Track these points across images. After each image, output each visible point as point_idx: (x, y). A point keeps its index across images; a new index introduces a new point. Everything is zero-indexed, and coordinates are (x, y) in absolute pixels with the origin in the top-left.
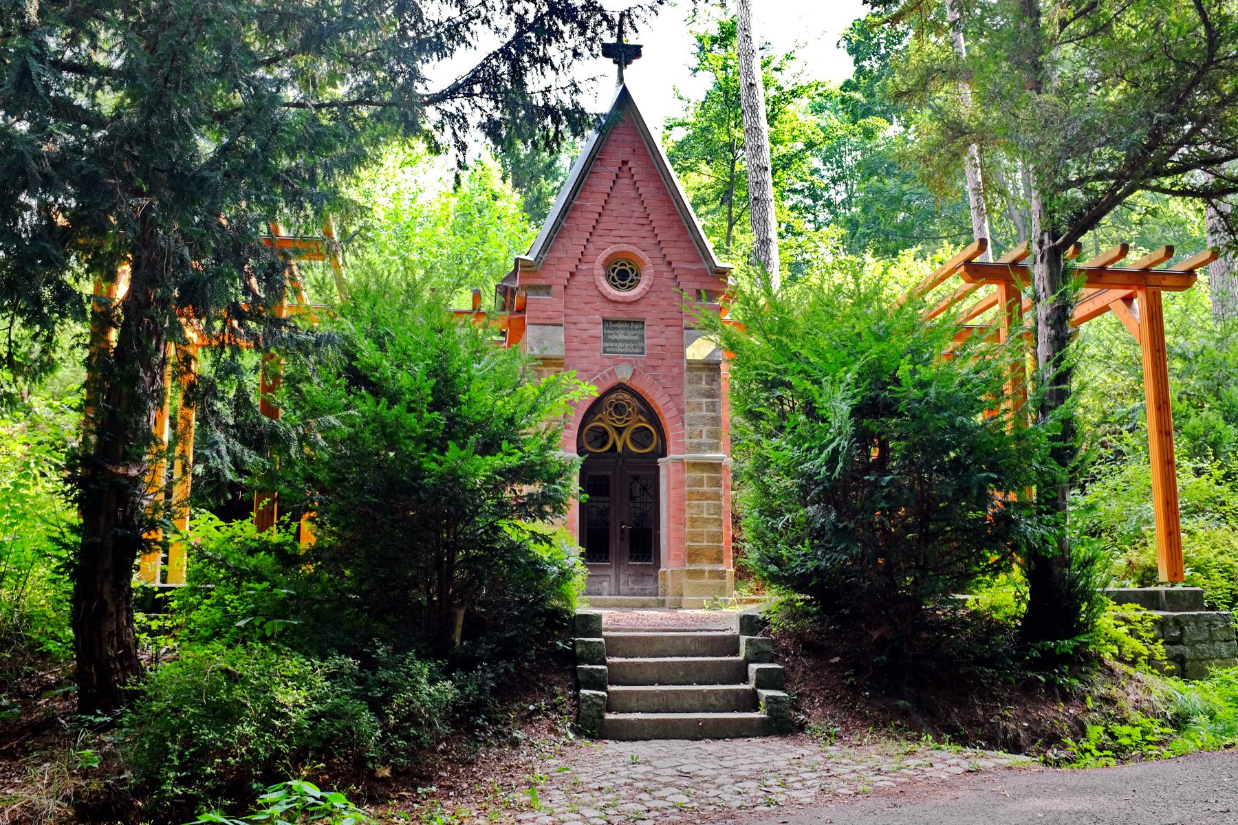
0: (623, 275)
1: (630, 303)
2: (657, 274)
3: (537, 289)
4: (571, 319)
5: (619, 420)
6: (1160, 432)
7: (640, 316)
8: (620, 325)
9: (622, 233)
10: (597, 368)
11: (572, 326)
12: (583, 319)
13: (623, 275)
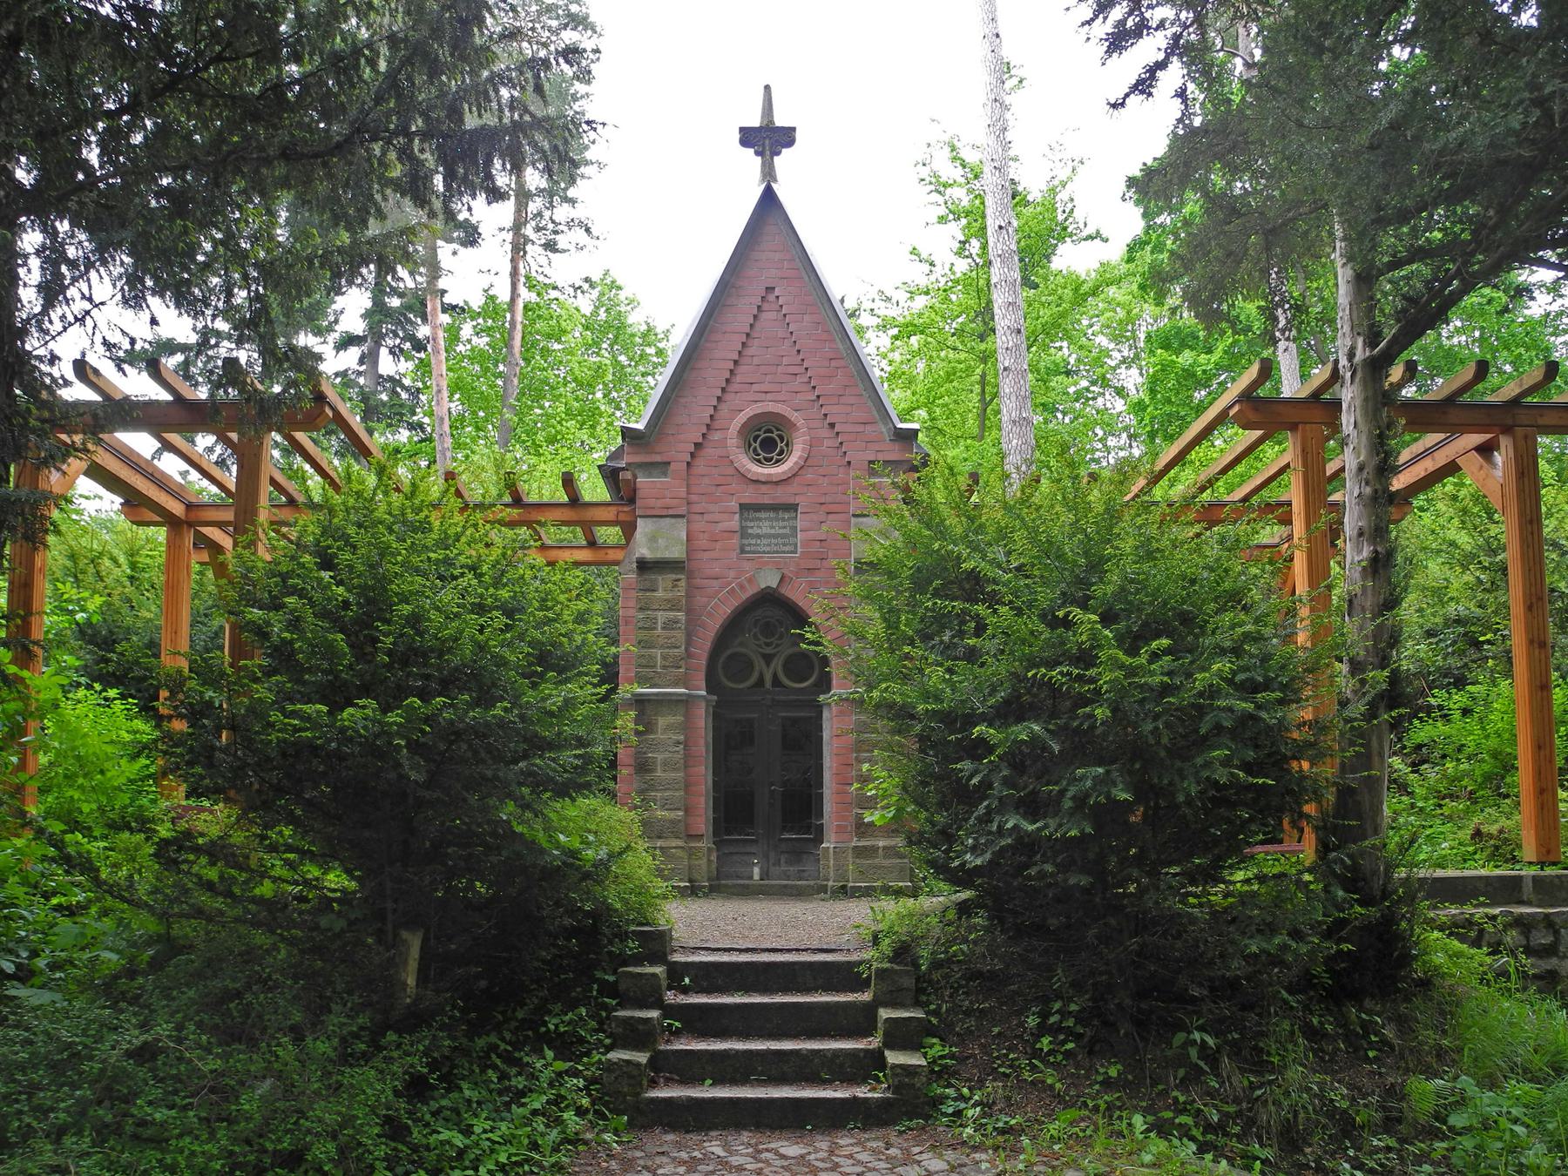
0: (769, 445)
1: (777, 483)
2: (813, 444)
3: (649, 467)
4: (697, 508)
5: (768, 645)
6: (1531, 642)
7: (791, 500)
8: (763, 515)
9: (764, 387)
10: (732, 574)
11: (698, 517)
12: (712, 507)
13: (769, 445)
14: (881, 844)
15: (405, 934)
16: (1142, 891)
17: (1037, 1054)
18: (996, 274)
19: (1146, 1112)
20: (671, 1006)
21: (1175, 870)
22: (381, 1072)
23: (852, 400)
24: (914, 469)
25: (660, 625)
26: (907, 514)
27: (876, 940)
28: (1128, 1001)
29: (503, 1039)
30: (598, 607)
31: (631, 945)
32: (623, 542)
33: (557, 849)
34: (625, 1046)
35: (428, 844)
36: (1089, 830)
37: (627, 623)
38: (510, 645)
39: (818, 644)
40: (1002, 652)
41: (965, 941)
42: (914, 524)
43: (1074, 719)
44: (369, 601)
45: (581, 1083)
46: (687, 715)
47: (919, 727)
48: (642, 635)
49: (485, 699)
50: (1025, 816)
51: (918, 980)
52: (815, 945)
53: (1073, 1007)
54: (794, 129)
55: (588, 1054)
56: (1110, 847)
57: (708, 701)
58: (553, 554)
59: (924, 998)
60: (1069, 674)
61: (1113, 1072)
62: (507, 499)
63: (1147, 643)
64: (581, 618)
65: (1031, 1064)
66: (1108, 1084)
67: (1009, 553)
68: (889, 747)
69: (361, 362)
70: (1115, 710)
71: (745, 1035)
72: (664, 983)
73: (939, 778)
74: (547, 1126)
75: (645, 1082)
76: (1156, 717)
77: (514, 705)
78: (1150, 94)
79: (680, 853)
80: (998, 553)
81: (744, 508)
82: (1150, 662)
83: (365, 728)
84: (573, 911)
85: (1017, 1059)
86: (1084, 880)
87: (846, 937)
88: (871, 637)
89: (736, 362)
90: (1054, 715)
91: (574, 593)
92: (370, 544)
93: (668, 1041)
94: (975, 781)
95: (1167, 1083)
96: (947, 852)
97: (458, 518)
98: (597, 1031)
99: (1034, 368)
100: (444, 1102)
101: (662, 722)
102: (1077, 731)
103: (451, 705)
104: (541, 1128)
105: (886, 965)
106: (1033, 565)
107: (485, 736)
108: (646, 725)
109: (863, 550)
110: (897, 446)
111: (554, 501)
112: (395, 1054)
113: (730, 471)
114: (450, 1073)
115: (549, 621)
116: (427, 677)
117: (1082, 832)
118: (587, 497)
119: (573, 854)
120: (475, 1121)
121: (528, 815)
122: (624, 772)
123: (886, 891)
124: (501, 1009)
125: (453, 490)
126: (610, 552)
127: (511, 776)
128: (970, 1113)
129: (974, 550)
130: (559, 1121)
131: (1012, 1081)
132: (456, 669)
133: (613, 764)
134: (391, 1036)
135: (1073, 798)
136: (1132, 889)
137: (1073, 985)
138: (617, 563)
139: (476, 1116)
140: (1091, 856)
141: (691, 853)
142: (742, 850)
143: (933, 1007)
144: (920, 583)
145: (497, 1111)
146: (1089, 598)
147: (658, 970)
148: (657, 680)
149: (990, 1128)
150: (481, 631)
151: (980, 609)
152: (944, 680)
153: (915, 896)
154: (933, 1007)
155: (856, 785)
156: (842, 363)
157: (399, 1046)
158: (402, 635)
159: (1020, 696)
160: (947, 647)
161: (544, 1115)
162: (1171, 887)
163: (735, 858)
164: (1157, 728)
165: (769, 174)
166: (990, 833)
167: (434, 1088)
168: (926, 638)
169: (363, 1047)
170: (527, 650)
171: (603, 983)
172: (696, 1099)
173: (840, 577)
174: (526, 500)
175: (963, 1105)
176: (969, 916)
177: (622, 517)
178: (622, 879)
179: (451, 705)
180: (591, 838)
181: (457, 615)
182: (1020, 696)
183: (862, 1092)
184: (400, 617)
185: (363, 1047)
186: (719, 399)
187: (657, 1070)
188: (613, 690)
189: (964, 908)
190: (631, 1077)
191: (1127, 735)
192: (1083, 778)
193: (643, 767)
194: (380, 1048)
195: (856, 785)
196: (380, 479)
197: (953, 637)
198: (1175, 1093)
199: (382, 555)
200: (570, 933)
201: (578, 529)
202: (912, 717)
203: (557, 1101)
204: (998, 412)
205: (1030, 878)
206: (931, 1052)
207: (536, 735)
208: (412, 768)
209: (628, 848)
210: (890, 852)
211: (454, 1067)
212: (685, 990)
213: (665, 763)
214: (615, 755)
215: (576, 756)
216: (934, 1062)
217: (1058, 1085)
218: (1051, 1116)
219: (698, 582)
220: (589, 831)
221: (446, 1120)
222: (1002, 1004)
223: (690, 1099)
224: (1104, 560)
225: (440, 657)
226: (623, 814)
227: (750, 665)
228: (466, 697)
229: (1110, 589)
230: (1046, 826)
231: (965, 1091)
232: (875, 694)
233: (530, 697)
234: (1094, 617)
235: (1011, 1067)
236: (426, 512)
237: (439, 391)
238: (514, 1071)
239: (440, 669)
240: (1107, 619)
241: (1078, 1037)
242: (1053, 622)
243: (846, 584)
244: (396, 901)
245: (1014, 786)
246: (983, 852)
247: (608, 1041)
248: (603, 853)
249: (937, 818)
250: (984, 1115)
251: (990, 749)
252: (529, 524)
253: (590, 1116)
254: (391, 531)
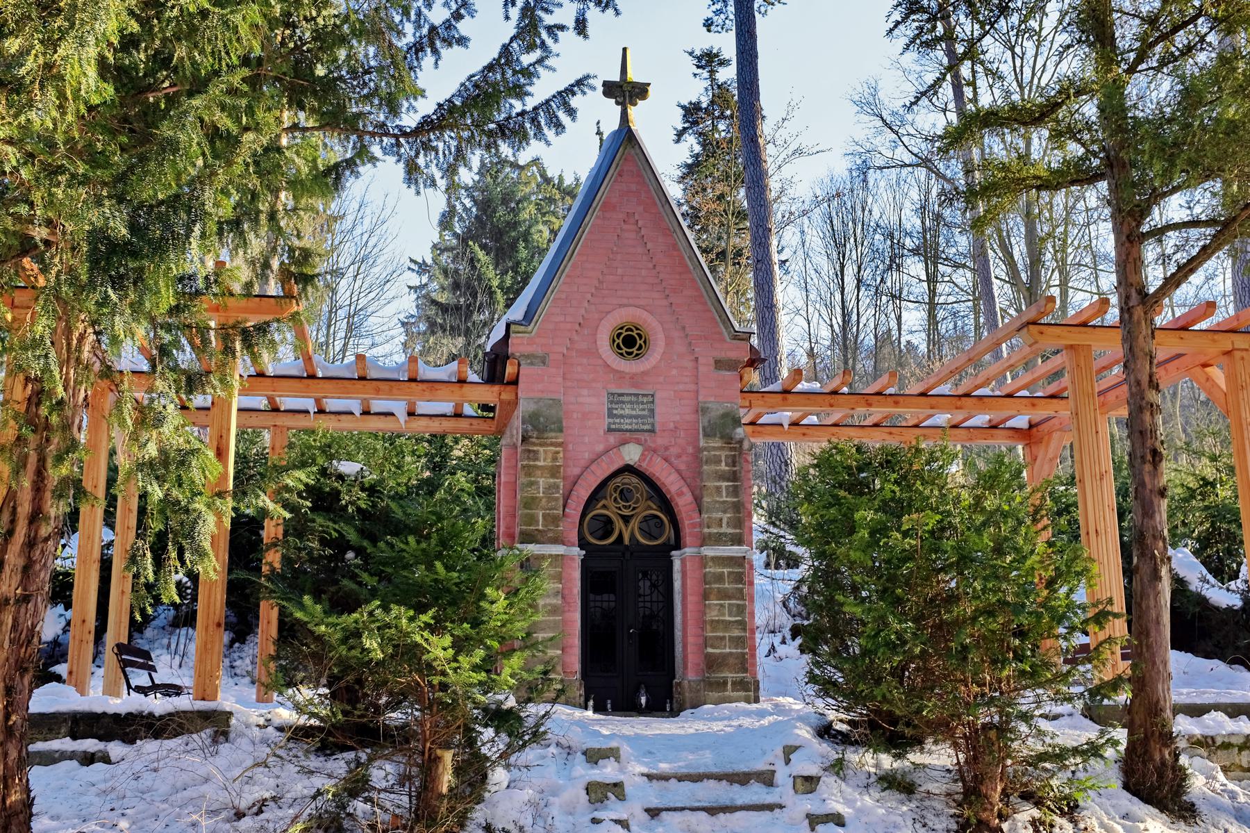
5: (625, 507)
165: (624, 117)
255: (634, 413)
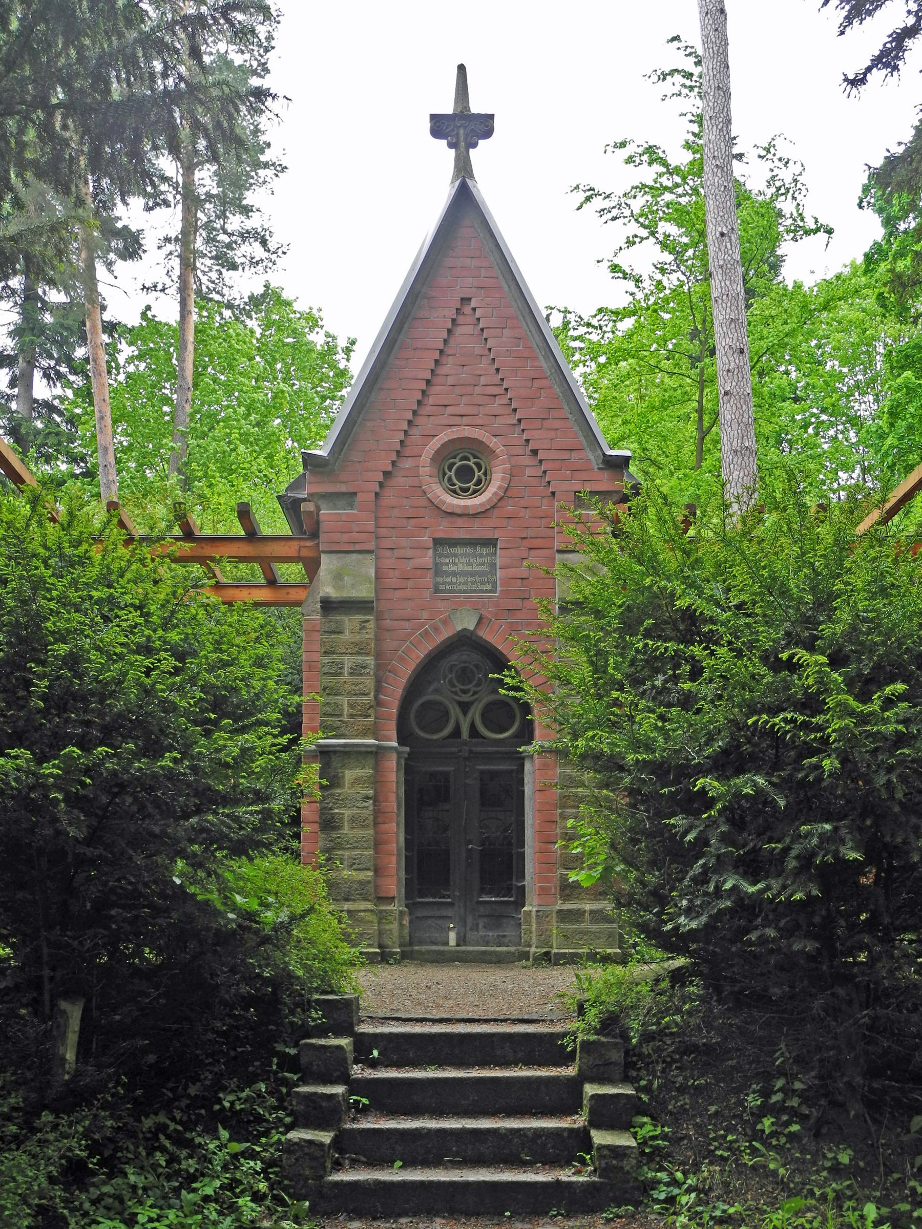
0: (465, 473)
1: (474, 516)
2: (513, 473)
4: (386, 543)
5: (465, 692)
7: (489, 535)
8: (459, 550)
10: (425, 615)
11: (388, 553)
12: (404, 542)
13: (465, 473)
14: (588, 907)
15: (64, 1005)
16: (873, 960)
17: (758, 1135)
18: (717, 286)
19: (879, 1203)
20: (357, 1081)
21: (909, 936)
22: (34, 1156)
23: (558, 424)
24: (625, 499)
25: (346, 670)
26: (616, 548)
27: (581, 1010)
28: (859, 1080)
29: (173, 1119)
30: (279, 651)
31: (314, 1015)
32: (307, 581)
33: (233, 911)
34: (308, 1124)
35: (89, 905)
36: (815, 892)
37: (310, 668)
38: (179, 689)
39: (518, 689)
40: (720, 697)
41: (679, 1011)
42: (623, 559)
43: (799, 771)
44: (21, 640)
45: (259, 1166)
46: (376, 768)
47: (627, 780)
48: (328, 681)
49: (153, 750)
50: (744, 875)
51: (627, 1053)
52: (516, 1015)
53: (798, 1085)
54: (491, 117)
55: (266, 1134)
56: (839, 912)
57: (399, 754)
58: (230, 593)
59: (634, 1074)
60: (794, 721)
61: (844, 1158)
62: (177, 531)
63: (880, 687)
64: (259, 662)
65: (751, 1147)
66: (837, 1170)
67: (728, 590)
68: (596, 802)
69: (12, 384)
70: (844, 761)
71: (438, 1112)
72: (350, 1057)
73: (649, 835)
74: (220, 1213)
75: (329, 1165)
76: (890, 769)
77: (184, 755)
78: (896, 68)
79: (368, 917)
80: (716, 589)
81: (438, 542)
82: (884, 709)
83: (17, 780)
84: (254, 979)
85: (736, 1141)
86: (810, 946)
87: (549, 1007)
88: (576, 682)
89: (428, 382)
90: (776, 766)
91: (254, 635)
92: (21, 577)
93: (354, 1120)
94: (690, 837)
95: (903, 1172)
96: (658, 915)
97: (123, 551)
98: (275, 1109)
99: (756, 393)
100: (106, 1189)
101: (349, 775)
102: (803, 783)
103: (114, 755)
104: (214, 1216)
105: (593, 1038)
106: (754, 603)
107: (152, 788)
108: (331, 781)
109: (566, 589)
110: (606, 475)
111: (231, 534)
112: (51, 1137)
113: (423, 502)
114: (113, 1157)
115: (226, 664)
116: (88, 724)
117: (808, 895)
118: (266, 531)
119: (251, 916)
120: (139, 1210)
121: (201, 874)
122: (306, 829)
123: (592, 957)
124: (171, 1085)
125: (115, 521)
126: (292, 591)
127: (181, 833)
128: (684, 1199)
129: (690, 586)
130: (233, 1208)
131: (731, 1166)
132: (120, 715)
133: (296, 821)
134: (47, 1117)
135: (797, 857)
136: (862, 958)
137: (798, 1060)
138: (299, 603)
139: (141, 1203)
140: (817, 919)
141: (382, 917)
142: (437, 913)
143: (643, 1083)
144: (629, 625)
145: (165, 1197)
146: (817, 638)
147: (344, 1042)
148: (343, 730)
149: (706, 1217)
150: (147, 674)
151: (696, 650)
152: (656, 728)
153: (624, 963)
154: (643, 1083)
155: (560, 843)
156: (544, 383)
157: (55, 1127)
158: (58, 678)
159: (739, 746)
160: (660, 693)
161: (216, 1201)
162: (906, 956)
163: (430, 922)
164: (889, 781)
165: (463, 169)
166: (706, 894)
167: (94, 1173)
168: (636, 682)
169: (13, 1129)
170: (199, 694)
171: (283, 1056)
172: (384, 1183)
173: (544, 618)
174: (197, 533)
175: (676, 1191)
176: (683, 985)
177: (305, 553)
178: (304, 944)
179: (114, 755)
180: (271, 899)
181: (121, 657)
182: (739, 746)
183: (566, 1175)
184: (56, 657)
185: (13, 1129)
186: (410, 422)
187: (342, 1151)
188: (294, 741)
189: (677, 976)
190: (313, 1158)
191: (857, 789)
192: (808, 835)
193: (328, 824)
194: (33, 1130)
195: (560, 843)
196: (33, 509)
197: (666, 681)
198: (912, 1183)
199: (35, 589)
200: (247, 1002)
201: (257, 566)
202: (621, 768)
203: (231, 1185)
204: (716, 442)
205: (750, 943)
206: (641, 1132)
207: (209, 788)
208: (70, 824)
209: (312, 910)
210: (598, 916)
211: (117, 1149)
212: (373, 1064)
213: (353, 820)
214: (298, 811)
215: (252, 813)
216: (645, 1143)
217: (782, 1171)
218: (774, 1204)
219: (388, 623)
220: (269, 892)
221: (108, 1208)
222: (718, 1081)
223: (378, 1183)
224: (833, 596)
225: (102, 702)
226: (308, 873)
227: (445, 715)
228: (132, 746)
229: (839, 628)
230: (768, 888)
231: (679, 1175)
232: (581, 743)
233: (202, 747)
234: (823, 659)
235: (729, 1149)
236: (85, 546)
237: (102, 418)
238: (184, 1153)
239: (101, 714)
240: (836, 661)
241: (803, 1119)
242: (777, 665)
243: (549, 625)
244: (53, 969)
245: (733, 843)
246: (698, 915)
247: (288, 1120)
248: (284, 916)
249: (648, 878)
250: (699, 1202)
251: (709, 803)
252: (202, 560)
253: (268, 1202)
254: (47, 566)
255: (469, 568)
